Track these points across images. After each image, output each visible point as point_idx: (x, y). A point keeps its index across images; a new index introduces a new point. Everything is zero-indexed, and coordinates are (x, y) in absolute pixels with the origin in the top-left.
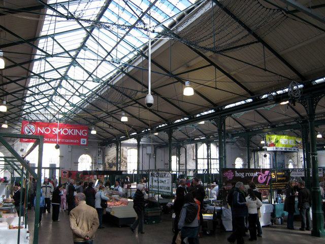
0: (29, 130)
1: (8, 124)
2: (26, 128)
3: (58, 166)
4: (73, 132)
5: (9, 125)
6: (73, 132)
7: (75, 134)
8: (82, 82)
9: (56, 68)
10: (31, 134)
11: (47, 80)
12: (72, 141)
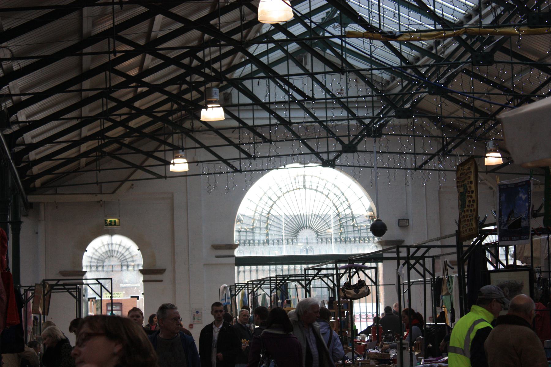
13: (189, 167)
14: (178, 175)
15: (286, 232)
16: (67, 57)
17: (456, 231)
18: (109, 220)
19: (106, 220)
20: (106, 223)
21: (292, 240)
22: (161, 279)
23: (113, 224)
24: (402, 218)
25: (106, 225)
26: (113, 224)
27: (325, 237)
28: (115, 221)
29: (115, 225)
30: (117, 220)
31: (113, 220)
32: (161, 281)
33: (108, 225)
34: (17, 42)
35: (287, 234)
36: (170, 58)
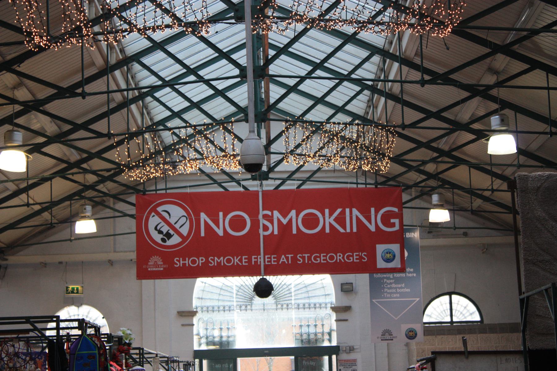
0: (165, 229)
1: (93, 217)
2: (154, 221)
3: (255, 279)
4: (341, 220)
5: (98, 216)
6: (341, 220)
7: (351, 227)
8: (291, 82)
9: (195, 100)
10: (175, 240)
11: (192, 78)
12: (339, 257)
13: (98, 227)
14: (85, 236)
15: (238, 300)
16: (57, 101)
17: (79, 330)
18: (71, 287)
19: (67, 288)
20: (67, 290)
21: (246, 307)
22: (345, 318)
23: (75, 291)
24: (345, 282)
25: (67, 293)
26: (75, 291)
27: (285, 302)
28: (77, 289)
29: (77, 293)
30: (80, 288)
31: (75, 287)
32: (346, 320)
33: (69, 293)
34: (98, 98)
35: (238, 300)
36: (64, 88)
